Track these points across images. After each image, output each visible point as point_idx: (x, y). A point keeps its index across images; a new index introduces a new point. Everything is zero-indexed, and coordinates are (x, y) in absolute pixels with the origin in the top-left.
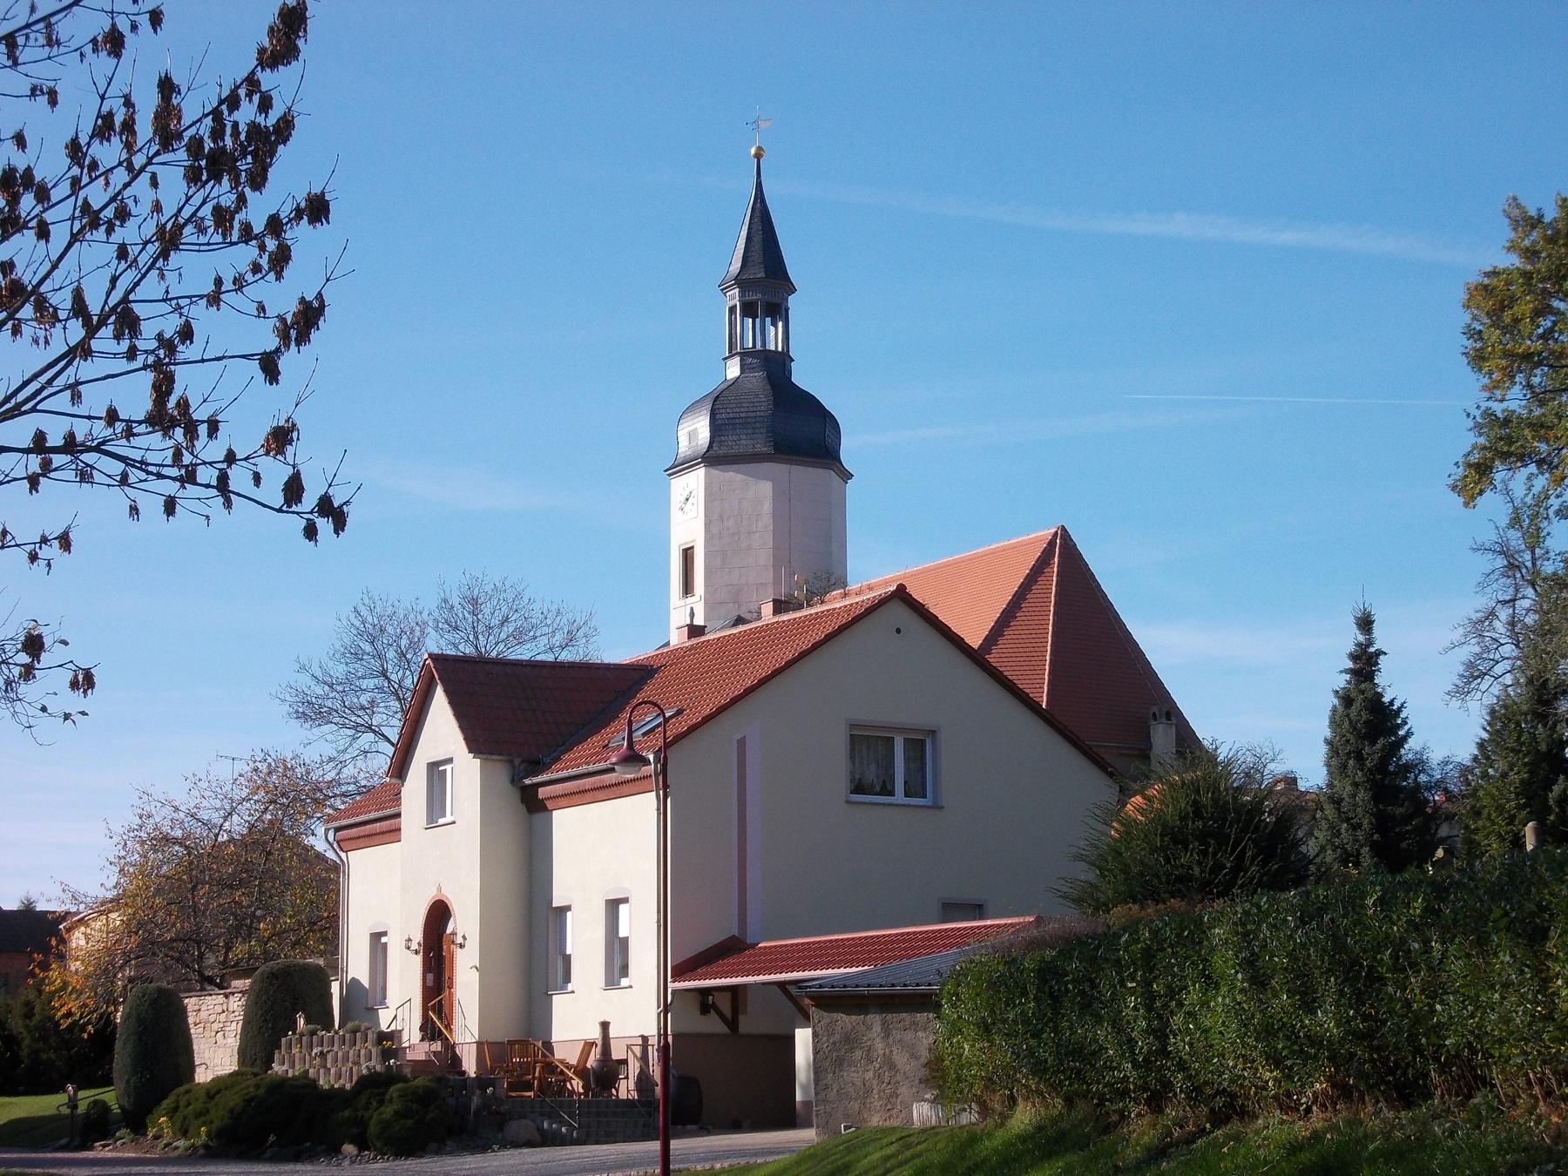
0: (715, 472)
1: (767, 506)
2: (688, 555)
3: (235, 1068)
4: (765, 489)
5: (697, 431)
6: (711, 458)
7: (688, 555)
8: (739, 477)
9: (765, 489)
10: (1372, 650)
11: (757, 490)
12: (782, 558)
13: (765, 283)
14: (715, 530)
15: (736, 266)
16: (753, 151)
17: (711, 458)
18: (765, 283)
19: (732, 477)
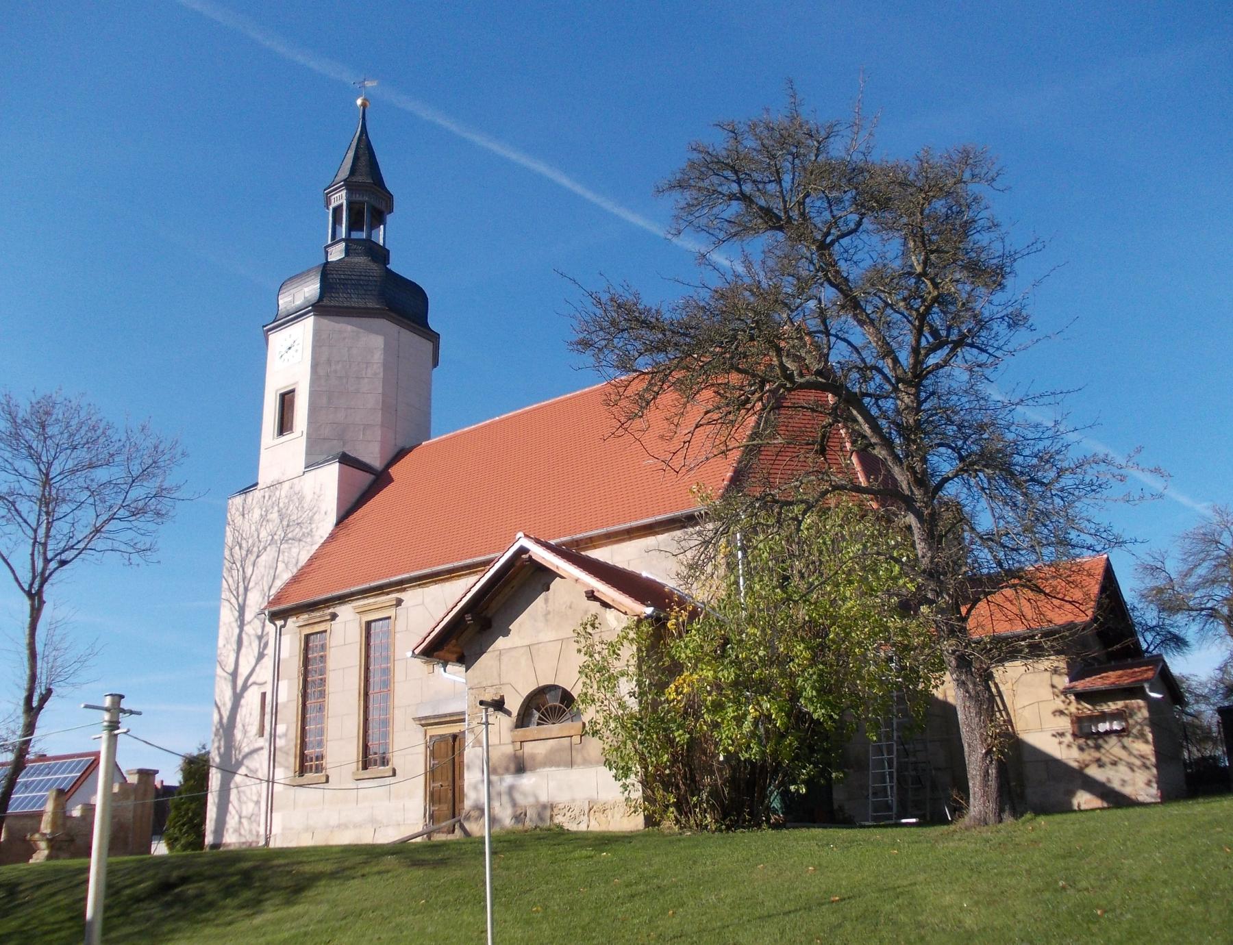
0: (325, 322)
1: (378, 357)
2: (284, 426)
3: (177, 784)
4: (378, 341)
5: (310, 289)
6: (319, 308)
7: (284, 426)
8: (349, 328)
9: (378, 341)
10: (688, 195)
11: (371, 342)
12: (388, 408)
13: (369, 200)
14: (321, 372)
15: (345, 172)
16: (359, 102)
17: (319, 308)
18: (369, 200)
19: (344, 328)
